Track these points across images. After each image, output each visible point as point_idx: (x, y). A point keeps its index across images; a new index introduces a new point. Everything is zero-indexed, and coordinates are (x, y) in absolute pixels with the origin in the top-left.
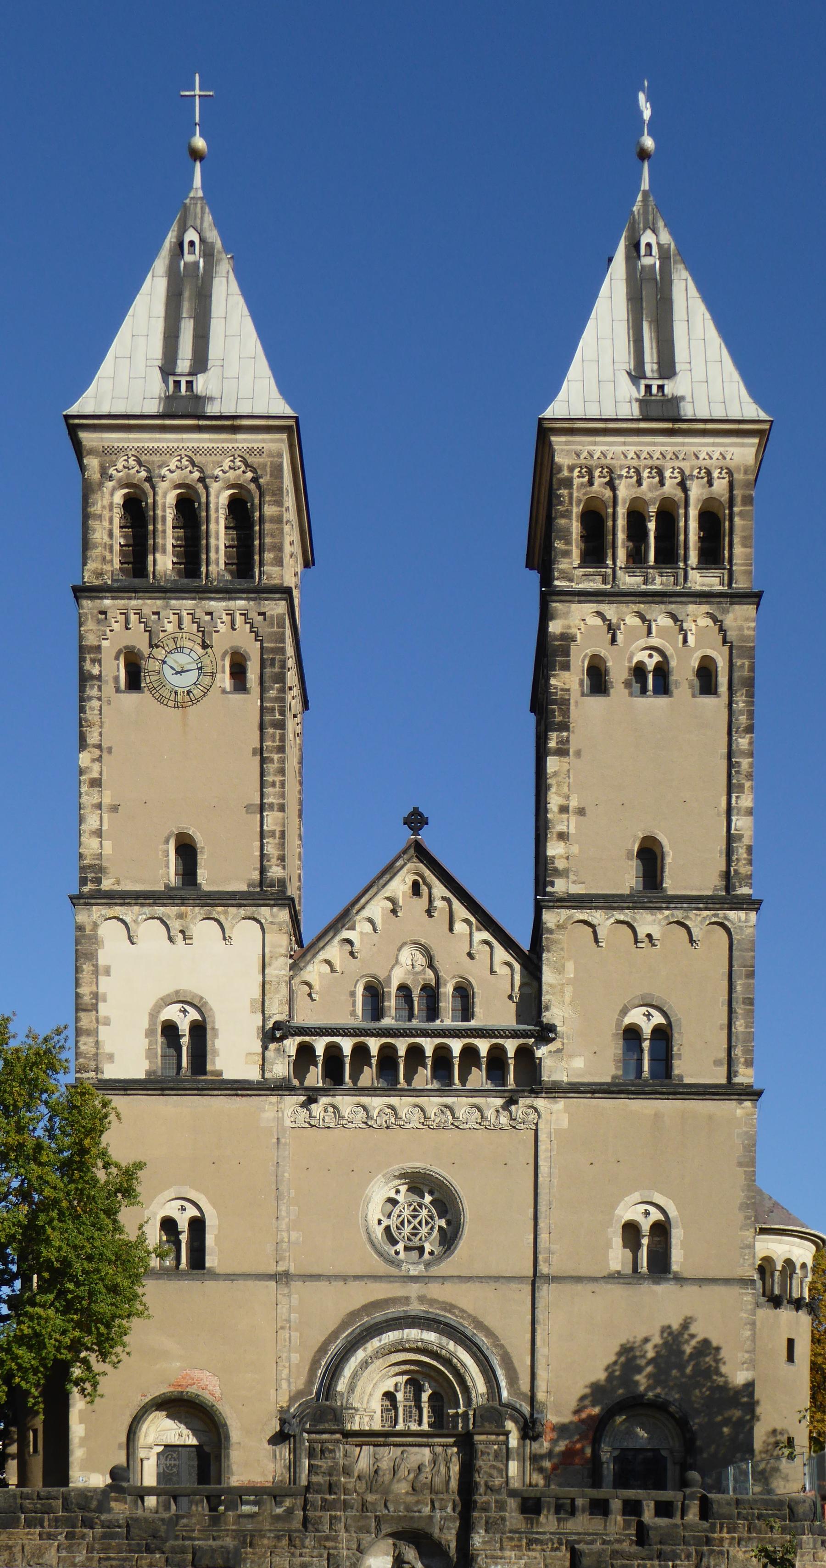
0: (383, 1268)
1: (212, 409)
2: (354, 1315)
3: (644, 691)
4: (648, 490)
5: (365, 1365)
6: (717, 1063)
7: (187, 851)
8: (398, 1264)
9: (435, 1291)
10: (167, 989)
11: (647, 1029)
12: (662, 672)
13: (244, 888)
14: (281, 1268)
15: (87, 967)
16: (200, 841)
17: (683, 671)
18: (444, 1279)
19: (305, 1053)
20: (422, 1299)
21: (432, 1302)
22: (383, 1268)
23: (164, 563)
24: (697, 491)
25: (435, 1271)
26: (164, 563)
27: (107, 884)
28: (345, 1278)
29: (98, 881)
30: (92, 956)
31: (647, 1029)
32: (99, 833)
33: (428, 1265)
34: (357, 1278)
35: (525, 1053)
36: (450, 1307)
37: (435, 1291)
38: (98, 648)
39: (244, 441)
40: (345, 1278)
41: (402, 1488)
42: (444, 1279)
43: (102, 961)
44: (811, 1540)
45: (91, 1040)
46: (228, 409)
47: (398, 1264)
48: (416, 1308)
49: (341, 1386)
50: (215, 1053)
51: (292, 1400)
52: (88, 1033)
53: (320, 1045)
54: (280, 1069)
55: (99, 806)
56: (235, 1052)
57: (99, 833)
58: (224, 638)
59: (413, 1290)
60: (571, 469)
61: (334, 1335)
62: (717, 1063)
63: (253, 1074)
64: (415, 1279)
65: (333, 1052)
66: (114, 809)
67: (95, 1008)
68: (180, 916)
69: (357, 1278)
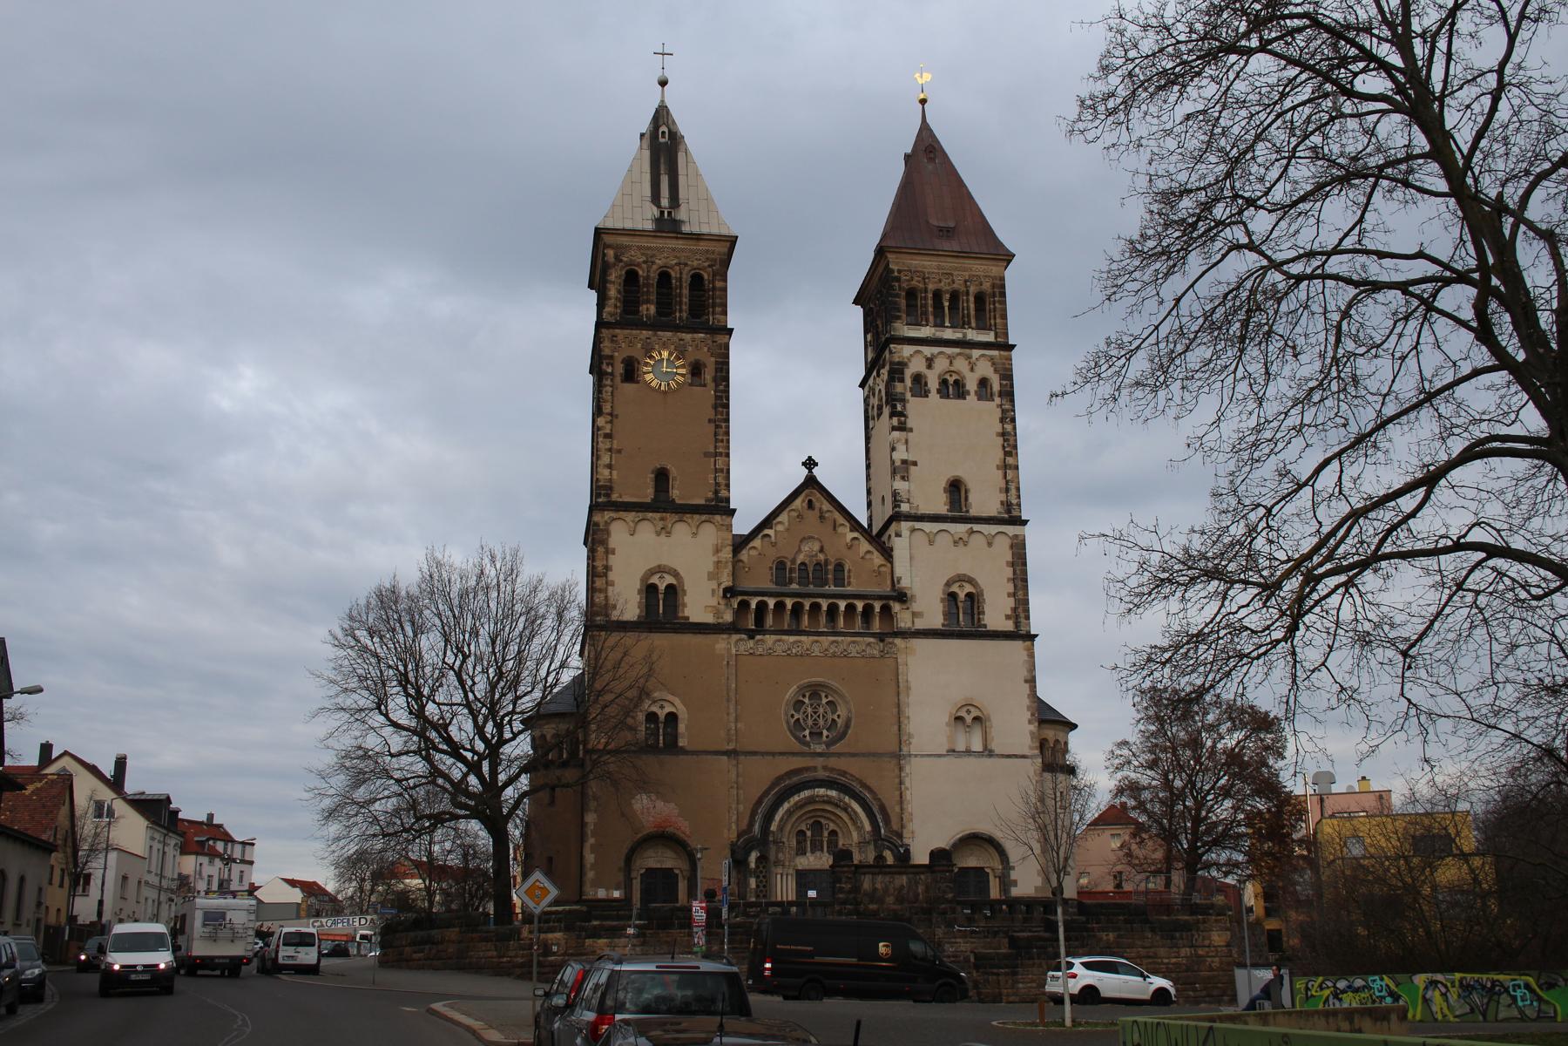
0: (798, 747)
1: (686, 229)
2: (780, 779)
3: (947, 396)
4: (944, 286)
5: (790, 813)
6: (1008, 617)
7: (662, 477)
8: (807, 744)
9: (833, 762)
10: (951, 574)
11: (662, 587)
12: (959, 384)
13: (702, 502)
14: (731, 746)
15: (601, 549)
16: (673, 472)
17: (971, 385)
18: (839, 755)
19: (744, 605)
20: (825, 768)
21: (832, 770)
22: (798, 747)
23: (682, 314)
24: (973, 289)
25: (833, 749)
26: (682, 314)
27: (615, 497)
28: (773, 754)
29: (608, 495)
30: (604, 542)
31: (662, 587)
32: (610, 466)
33: (828, 745)
34: (781, 754)
35: (886, 609)
36: (844, 773)
37: (833, 762)
38: (612, 357)
39: (703, 246)
40: (773, 754)
41: (890, 900)
42: (839, 755)
43: (611, 545)
44: (237, 950)
45: (602, 596)
46: (696, 230)
47: (807, 744)
48: (821, 774)
49: (773, 827)
50: (684, 605)
51: (739, 836)
52: (600, 591)
53: (860, 605)
54: (728, 617)
55: (610, 450)
56: (700, 604)
57: (610, 466)
58: (693, 354)
59: (819, 762)
60: (899, 271)
61: (766, 793)
62: (1008, 617)
63: (709, 619)
64: (820, 755)
65: (762, 606)
66: (619, 451)
67: (606, 575)
68: (662, 519)
69: (781, 754)
